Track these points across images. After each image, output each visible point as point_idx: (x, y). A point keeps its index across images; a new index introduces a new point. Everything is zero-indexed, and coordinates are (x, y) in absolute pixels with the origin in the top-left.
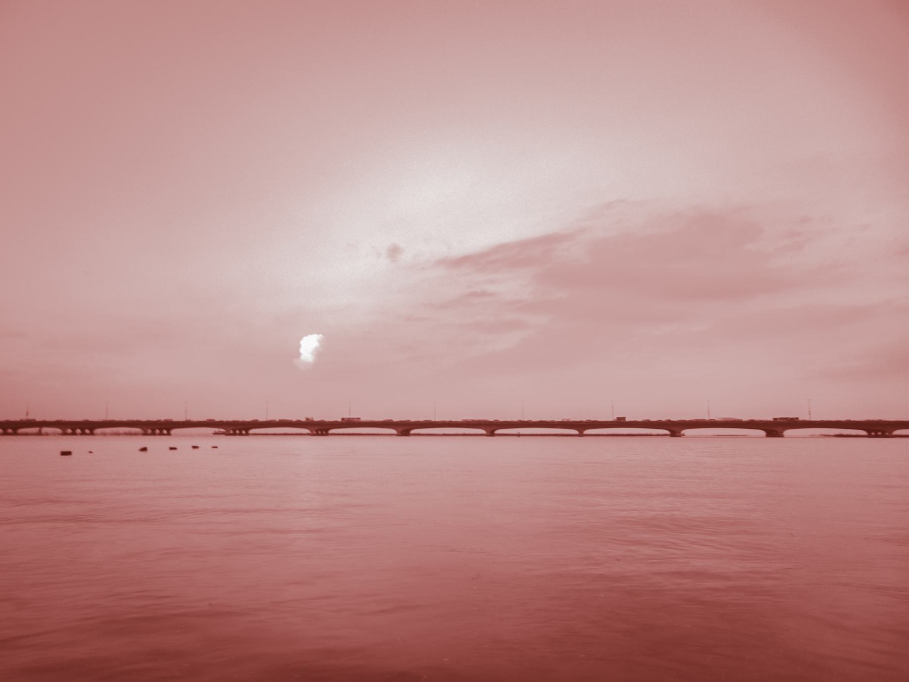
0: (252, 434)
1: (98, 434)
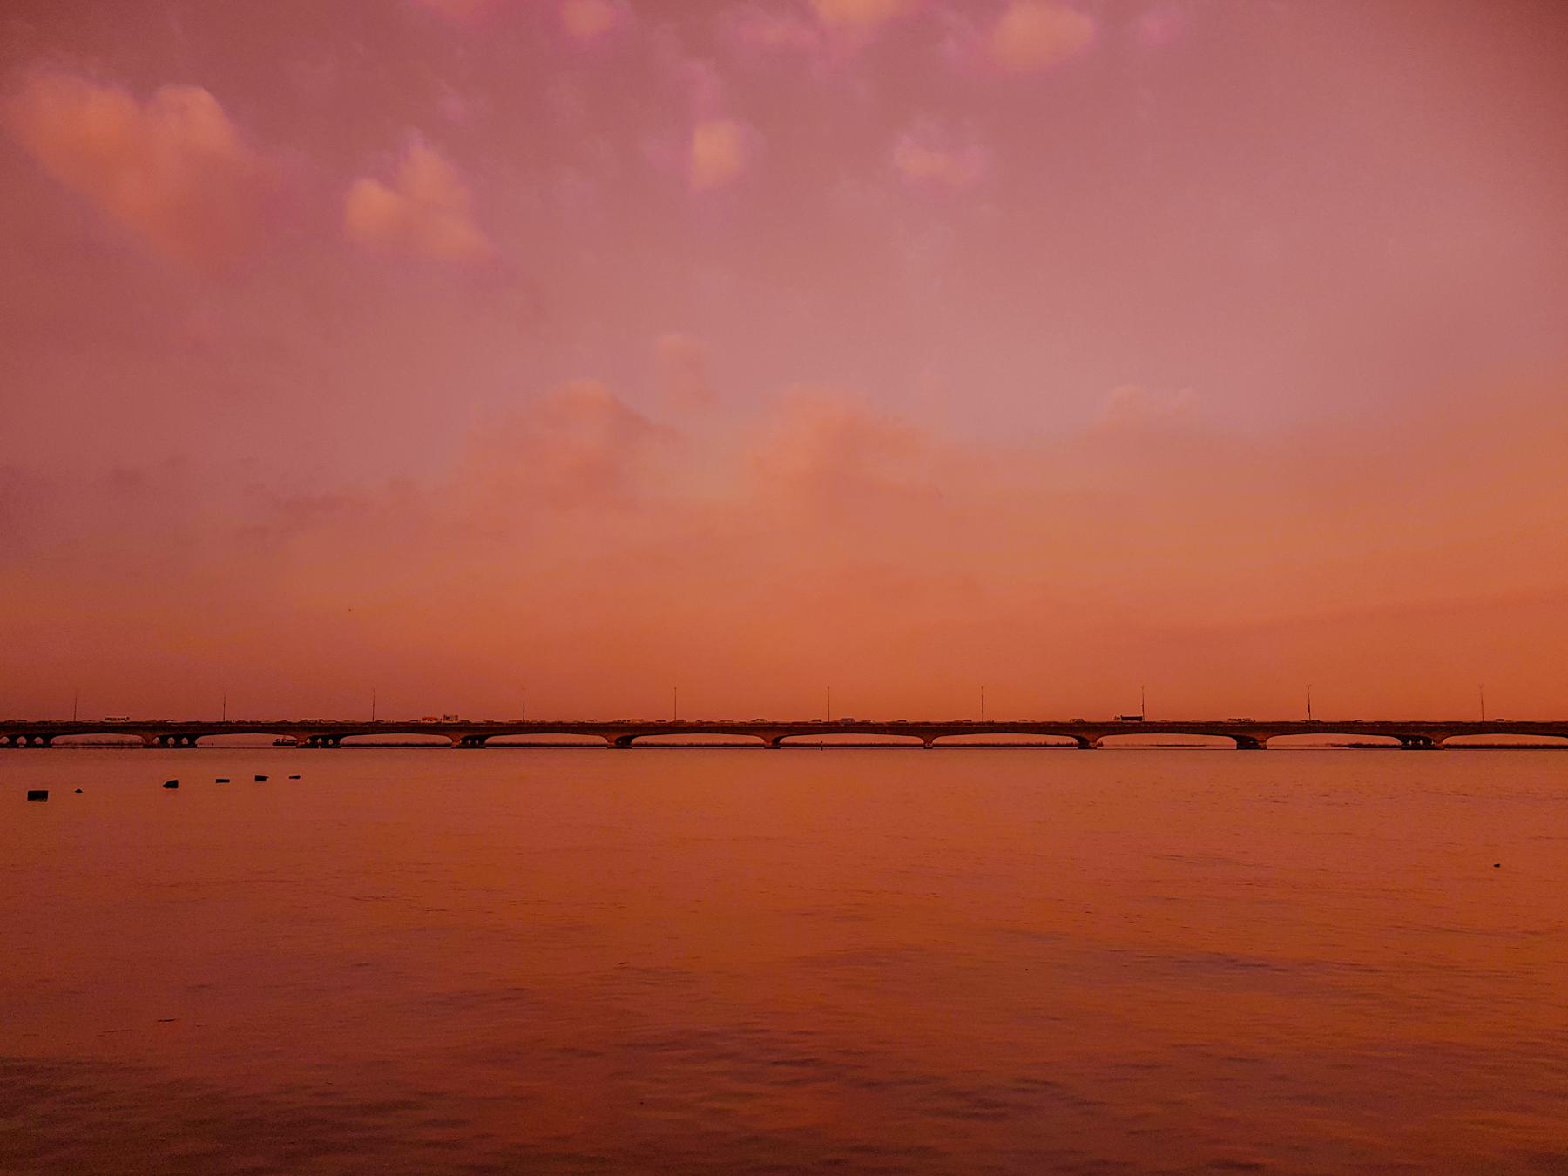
0: (344, 745)
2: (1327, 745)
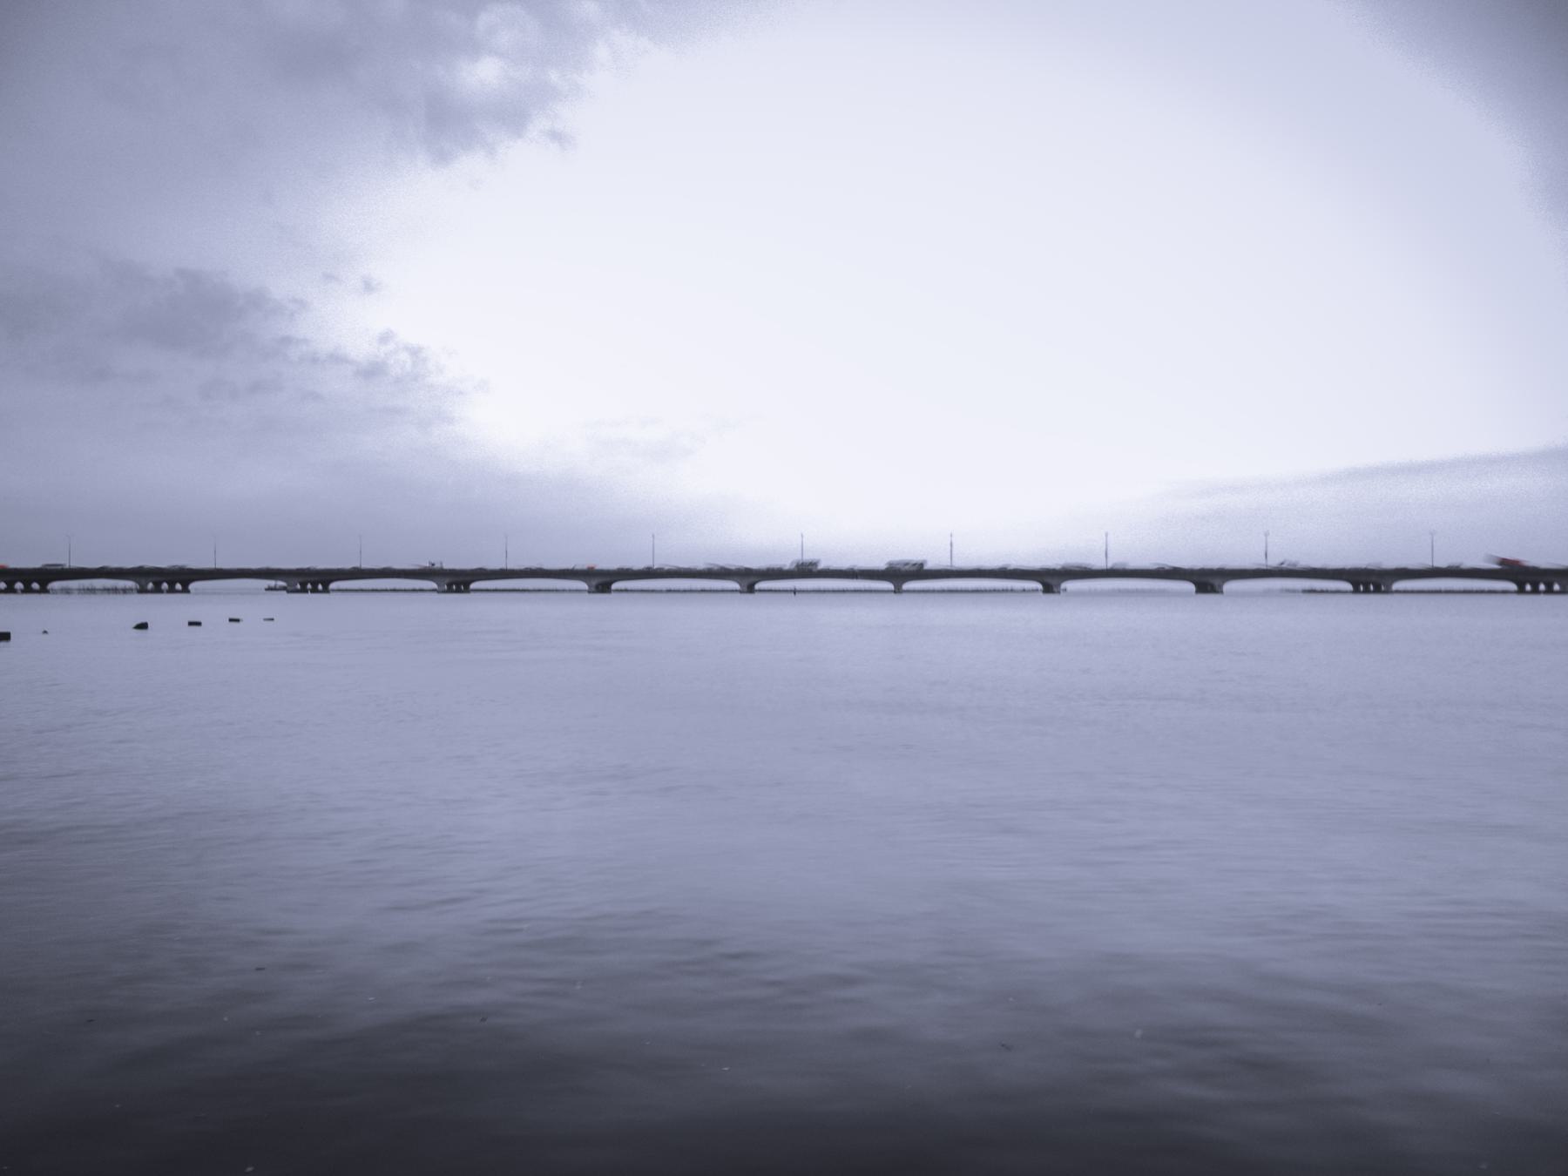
0: (1398, 592)
1: (55, 592)
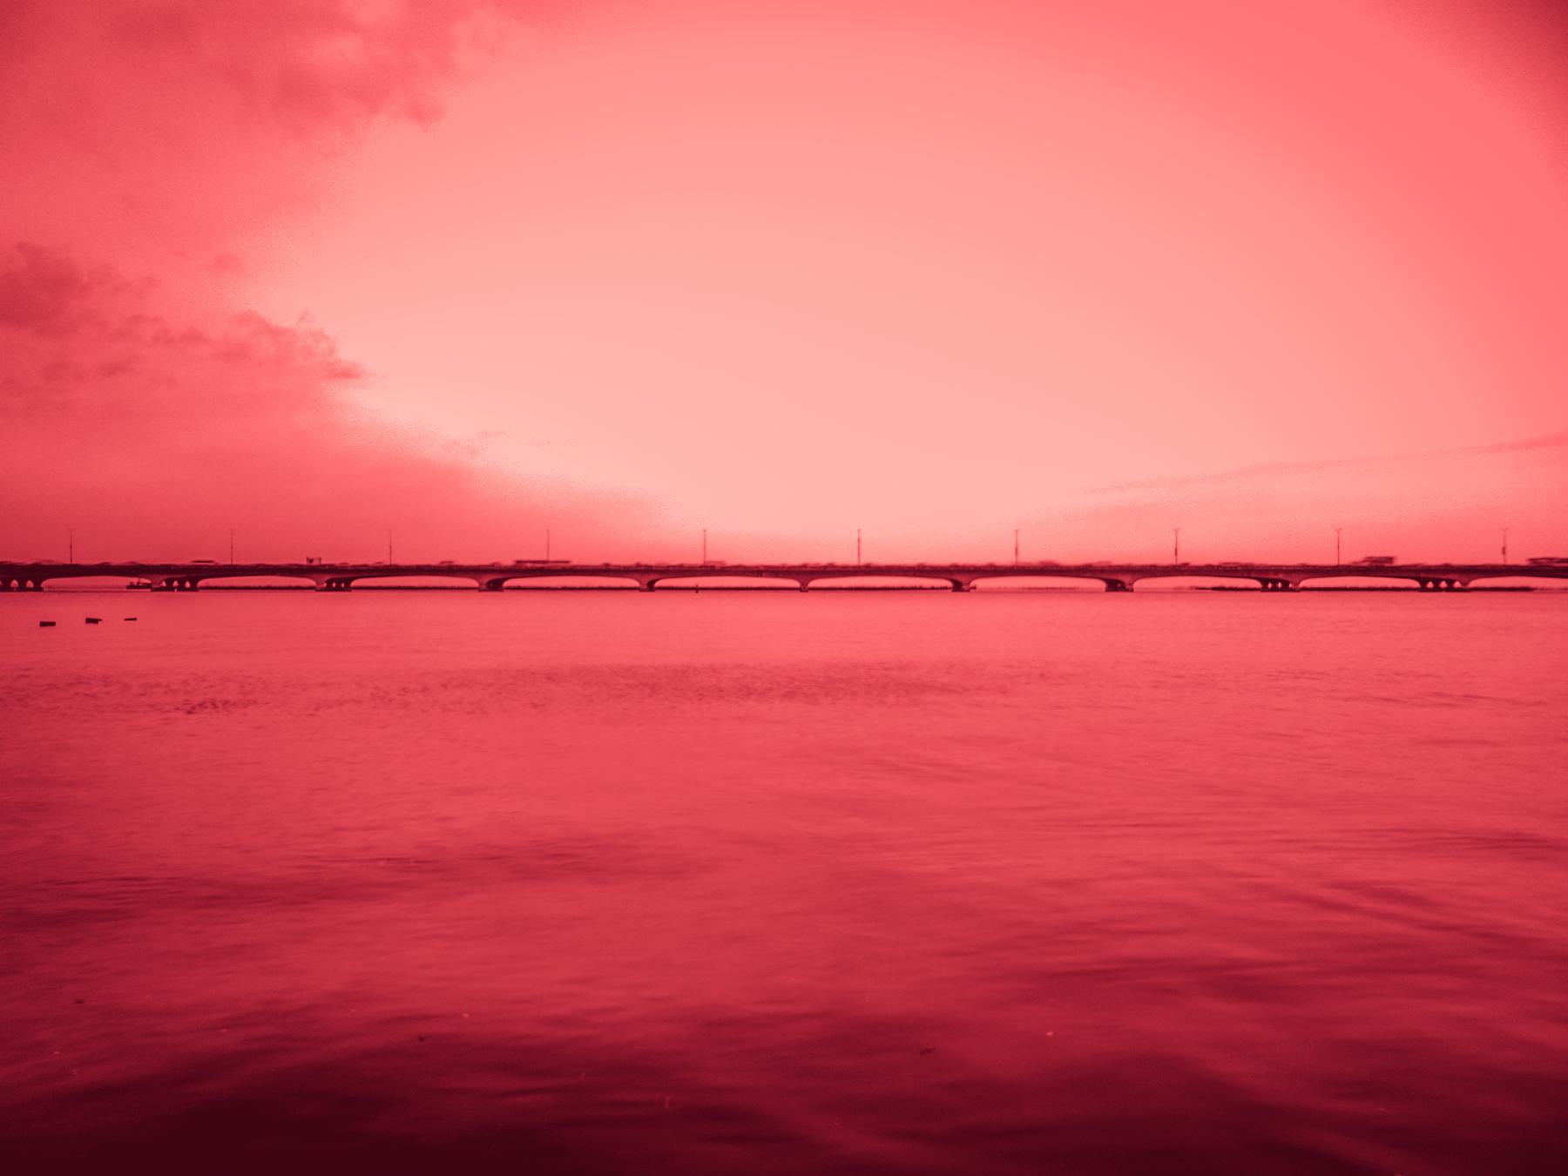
2: (1191, 588)
